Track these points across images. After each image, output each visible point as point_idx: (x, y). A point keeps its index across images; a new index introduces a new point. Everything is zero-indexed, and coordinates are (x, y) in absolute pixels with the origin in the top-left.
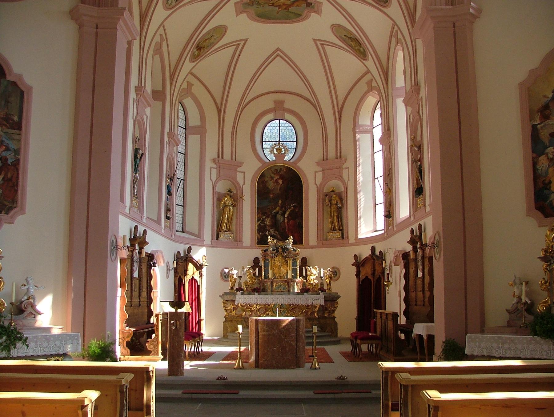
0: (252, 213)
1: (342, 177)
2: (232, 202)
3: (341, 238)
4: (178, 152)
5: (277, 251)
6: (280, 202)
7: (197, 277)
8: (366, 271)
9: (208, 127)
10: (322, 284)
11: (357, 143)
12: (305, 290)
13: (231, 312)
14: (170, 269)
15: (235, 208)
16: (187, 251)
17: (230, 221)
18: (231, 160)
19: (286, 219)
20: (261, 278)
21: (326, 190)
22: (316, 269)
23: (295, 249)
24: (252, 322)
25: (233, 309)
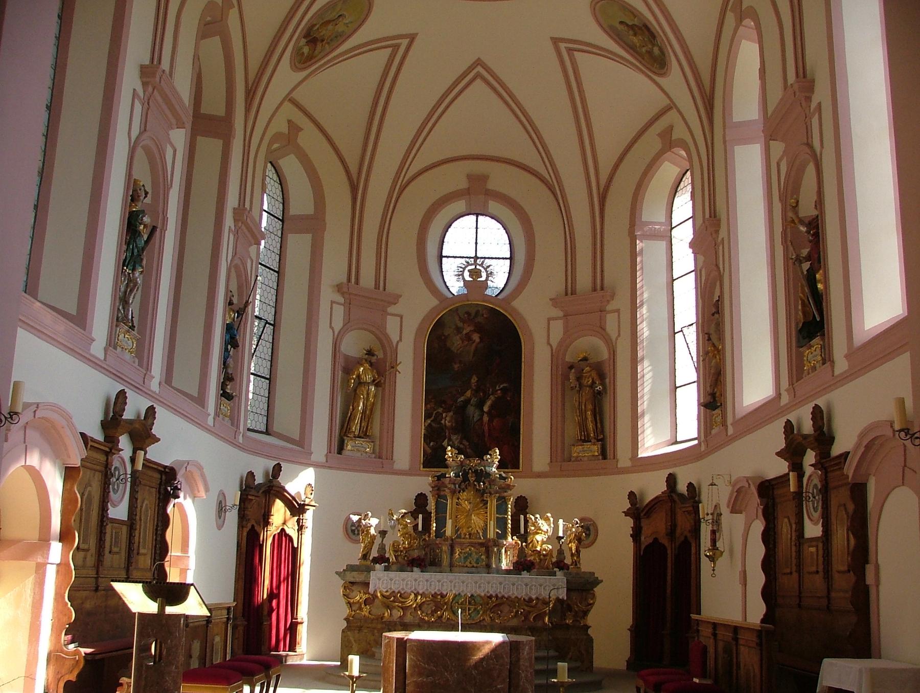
0: (414, 401)
1: (604, 330)
2: (374, 376)
3: (601, 457)
4: (261, 264)
5: (465, 479)
6: (474, 380)
7: (292, 531)
8: (656, 527)
9: (328, 218)
10: (561, 552)
11: (639, 259)
12: (522, 565)
13: (360, 609)
14: (228, 508)
15: (380, 389)
16: (271, 474)
17: (367, 416)
18: (375, 288)
19: (485, 415)
20: (429, 537)
21: (568, 359)
22: (549, 520)
23: (504, 475)
24: (388, 645)
25: (366, 602)
